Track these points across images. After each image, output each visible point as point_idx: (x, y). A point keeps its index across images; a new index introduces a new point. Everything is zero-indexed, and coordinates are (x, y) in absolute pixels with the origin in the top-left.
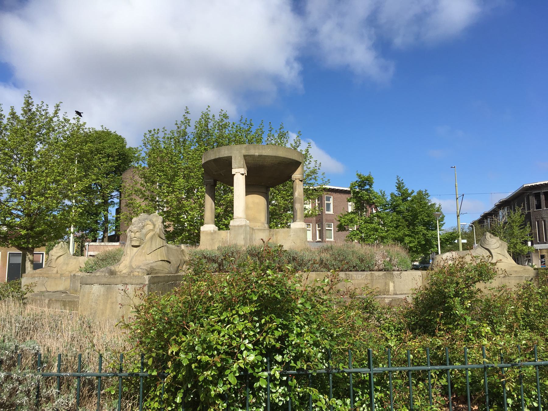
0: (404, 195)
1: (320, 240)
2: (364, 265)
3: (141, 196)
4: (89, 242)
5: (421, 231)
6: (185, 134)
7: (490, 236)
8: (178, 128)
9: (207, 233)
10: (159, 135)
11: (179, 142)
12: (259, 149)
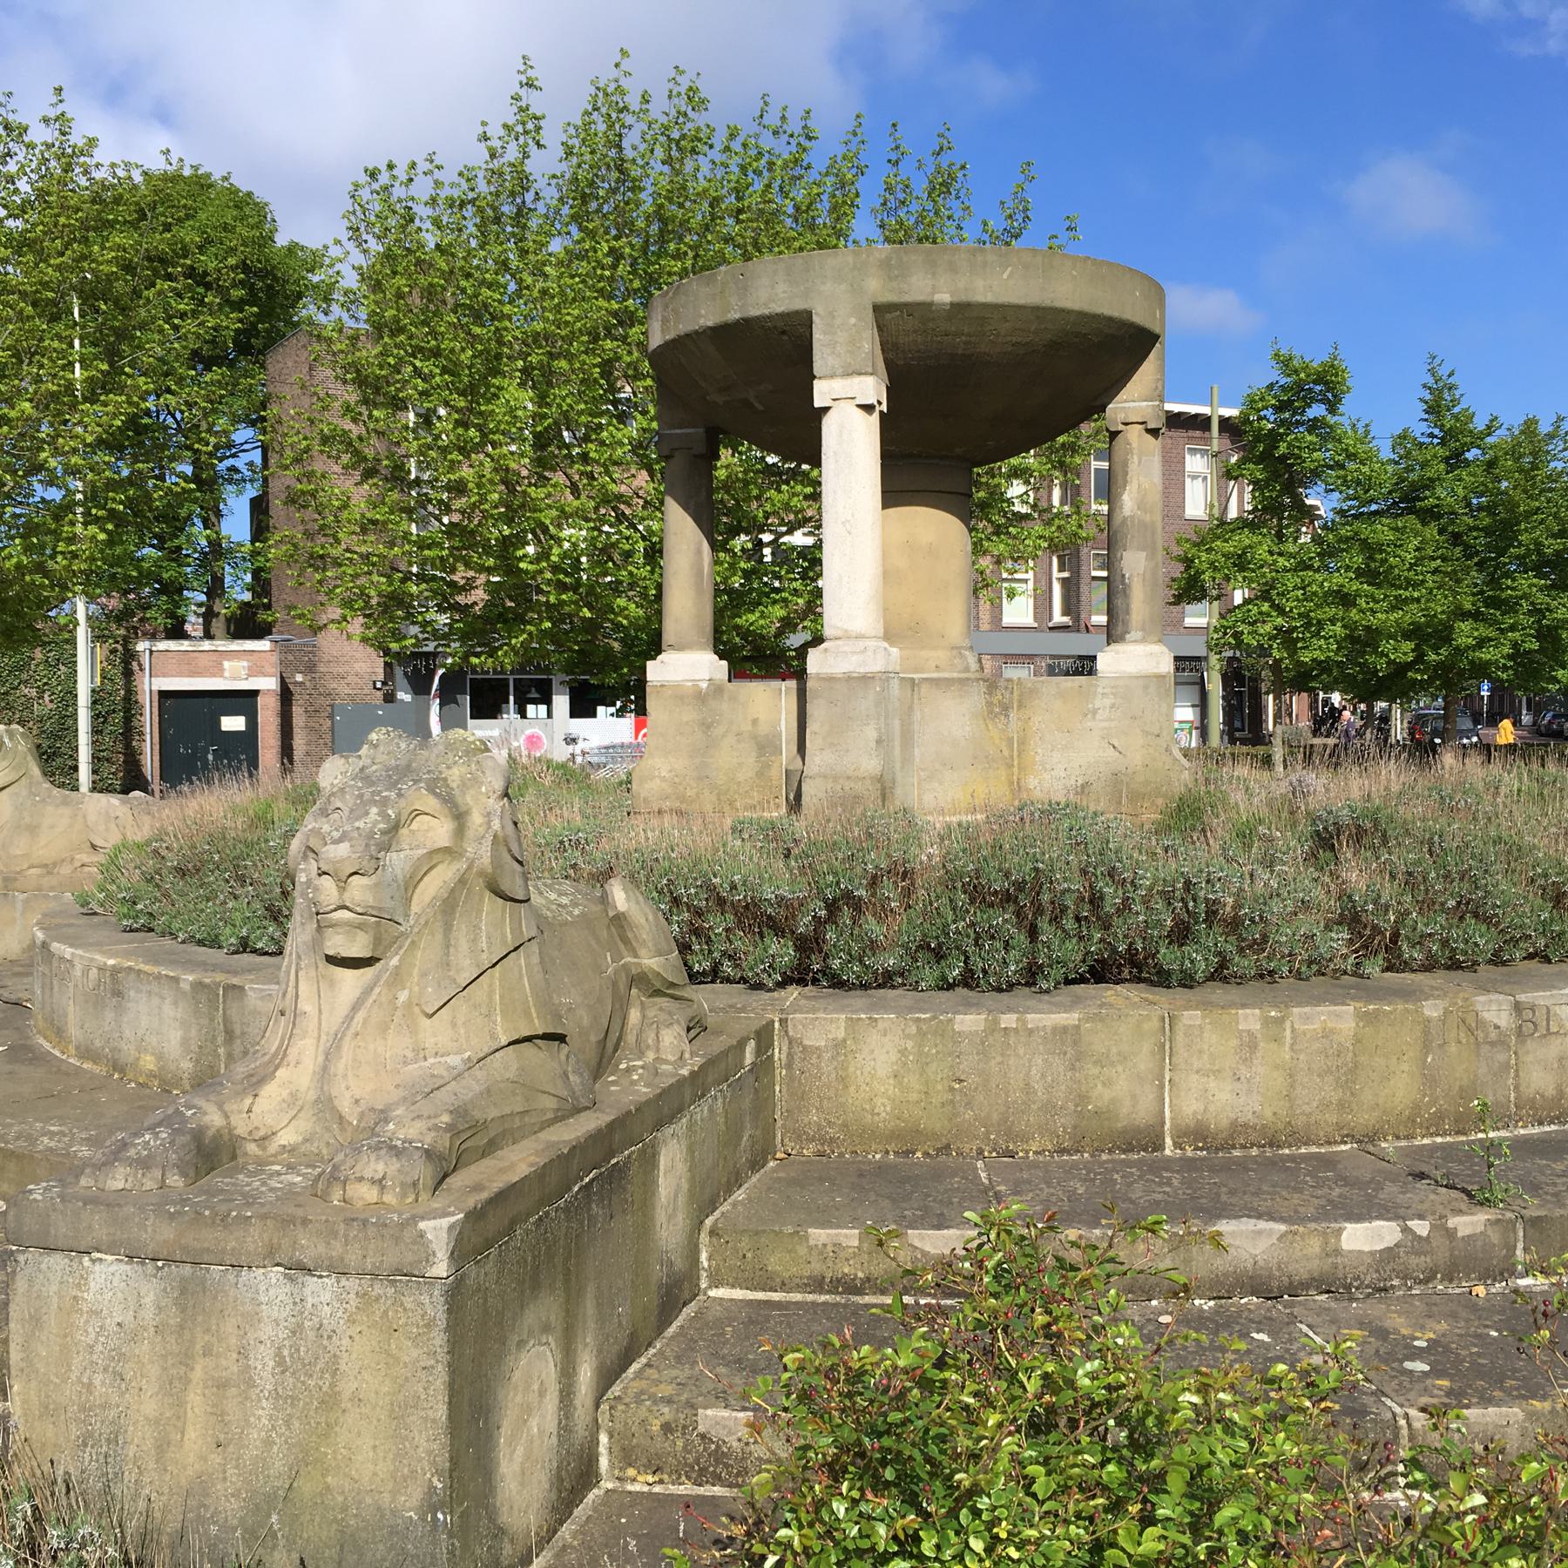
0: (1455, 439)
1: (1066, 620)
3: (346, 458)
4: (153, 636)
5: (1525, 596)
6: (523, 181)
8: (493, 156)
10: (414, 190)
11: (497, 220)
12: (953, 269)
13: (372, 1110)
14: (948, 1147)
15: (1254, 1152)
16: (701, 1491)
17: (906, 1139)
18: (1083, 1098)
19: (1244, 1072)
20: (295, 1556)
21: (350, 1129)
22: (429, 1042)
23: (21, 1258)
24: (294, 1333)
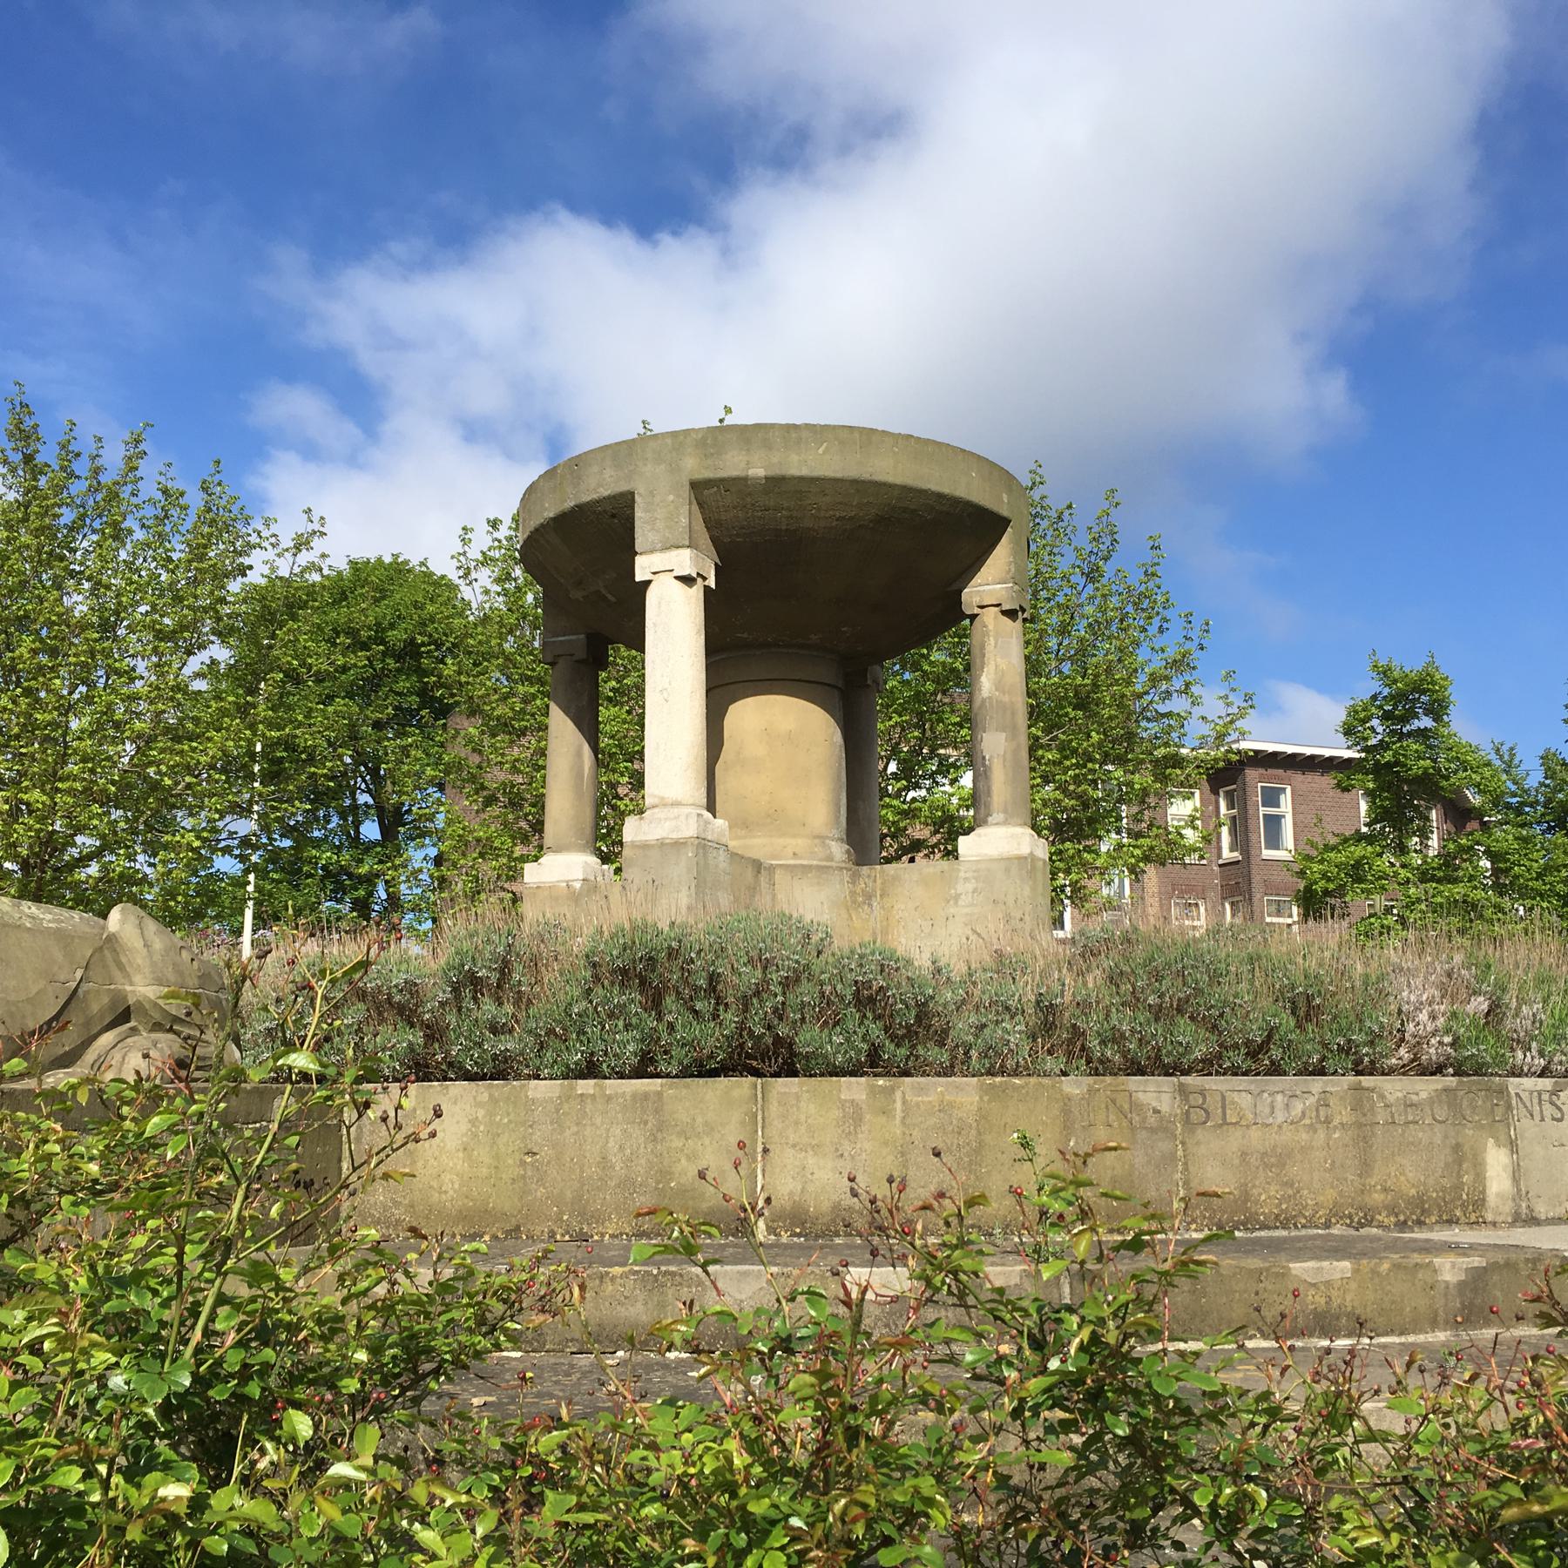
2: (1314, 1037)
14: (517, 1228)
19: (846, 1147)
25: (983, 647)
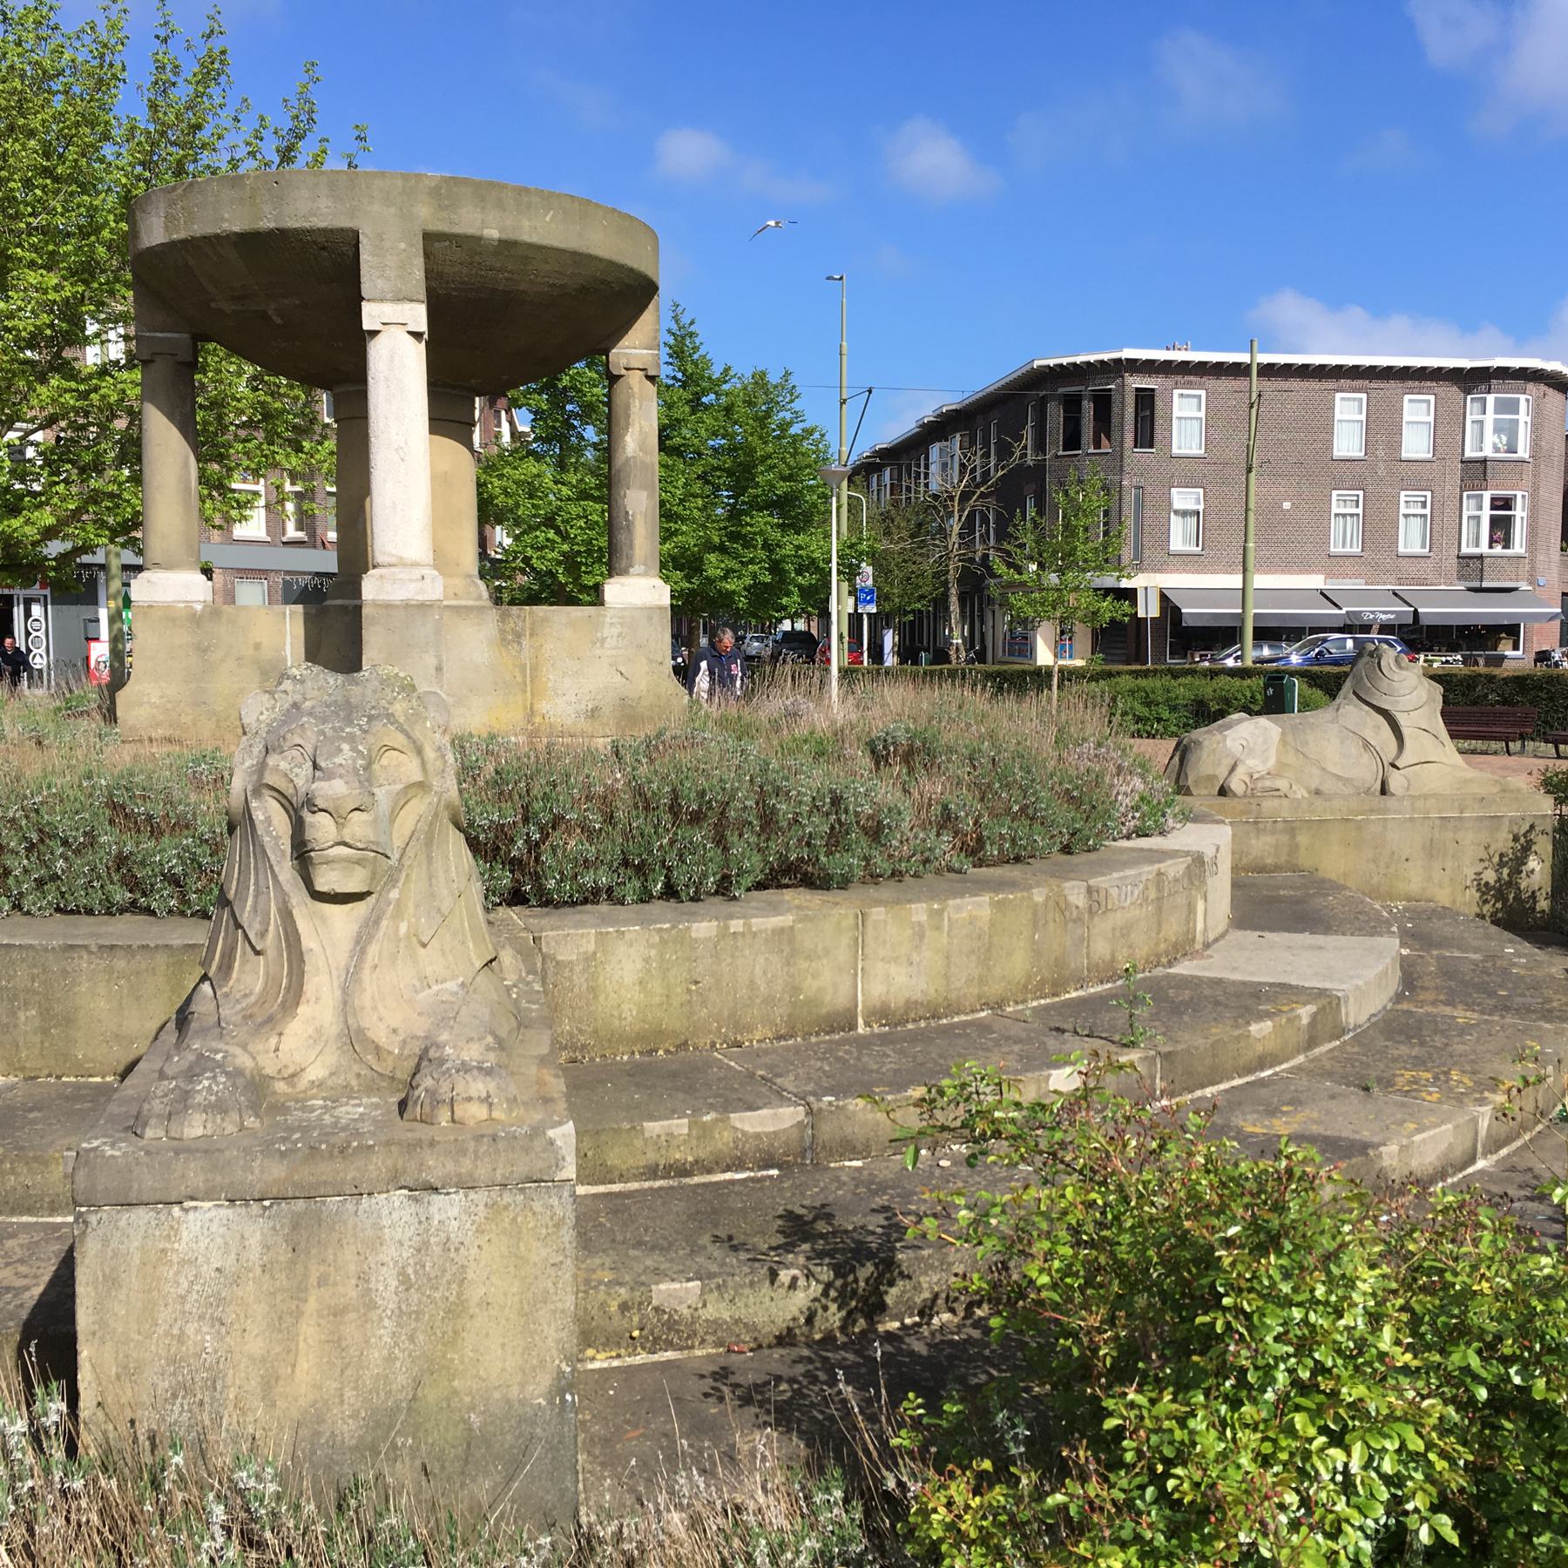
1: (301, 535)
5: (761, 533)
7: (1397, 660)
9: (169, 616)
13: (414, 1037)
15: (923, 1024)
16: (656, 1357)
17: (649, 1039)
18: (796, 990)
19: (915, 958)
20: (418, 1463)
21: (390, 1059)
22: (429, 971)
23: (93, 1219)
24: (419, 1251)
25: (628, 407)
